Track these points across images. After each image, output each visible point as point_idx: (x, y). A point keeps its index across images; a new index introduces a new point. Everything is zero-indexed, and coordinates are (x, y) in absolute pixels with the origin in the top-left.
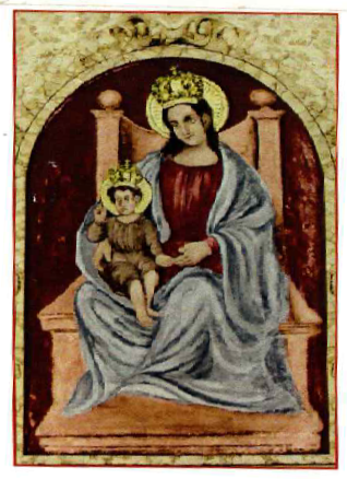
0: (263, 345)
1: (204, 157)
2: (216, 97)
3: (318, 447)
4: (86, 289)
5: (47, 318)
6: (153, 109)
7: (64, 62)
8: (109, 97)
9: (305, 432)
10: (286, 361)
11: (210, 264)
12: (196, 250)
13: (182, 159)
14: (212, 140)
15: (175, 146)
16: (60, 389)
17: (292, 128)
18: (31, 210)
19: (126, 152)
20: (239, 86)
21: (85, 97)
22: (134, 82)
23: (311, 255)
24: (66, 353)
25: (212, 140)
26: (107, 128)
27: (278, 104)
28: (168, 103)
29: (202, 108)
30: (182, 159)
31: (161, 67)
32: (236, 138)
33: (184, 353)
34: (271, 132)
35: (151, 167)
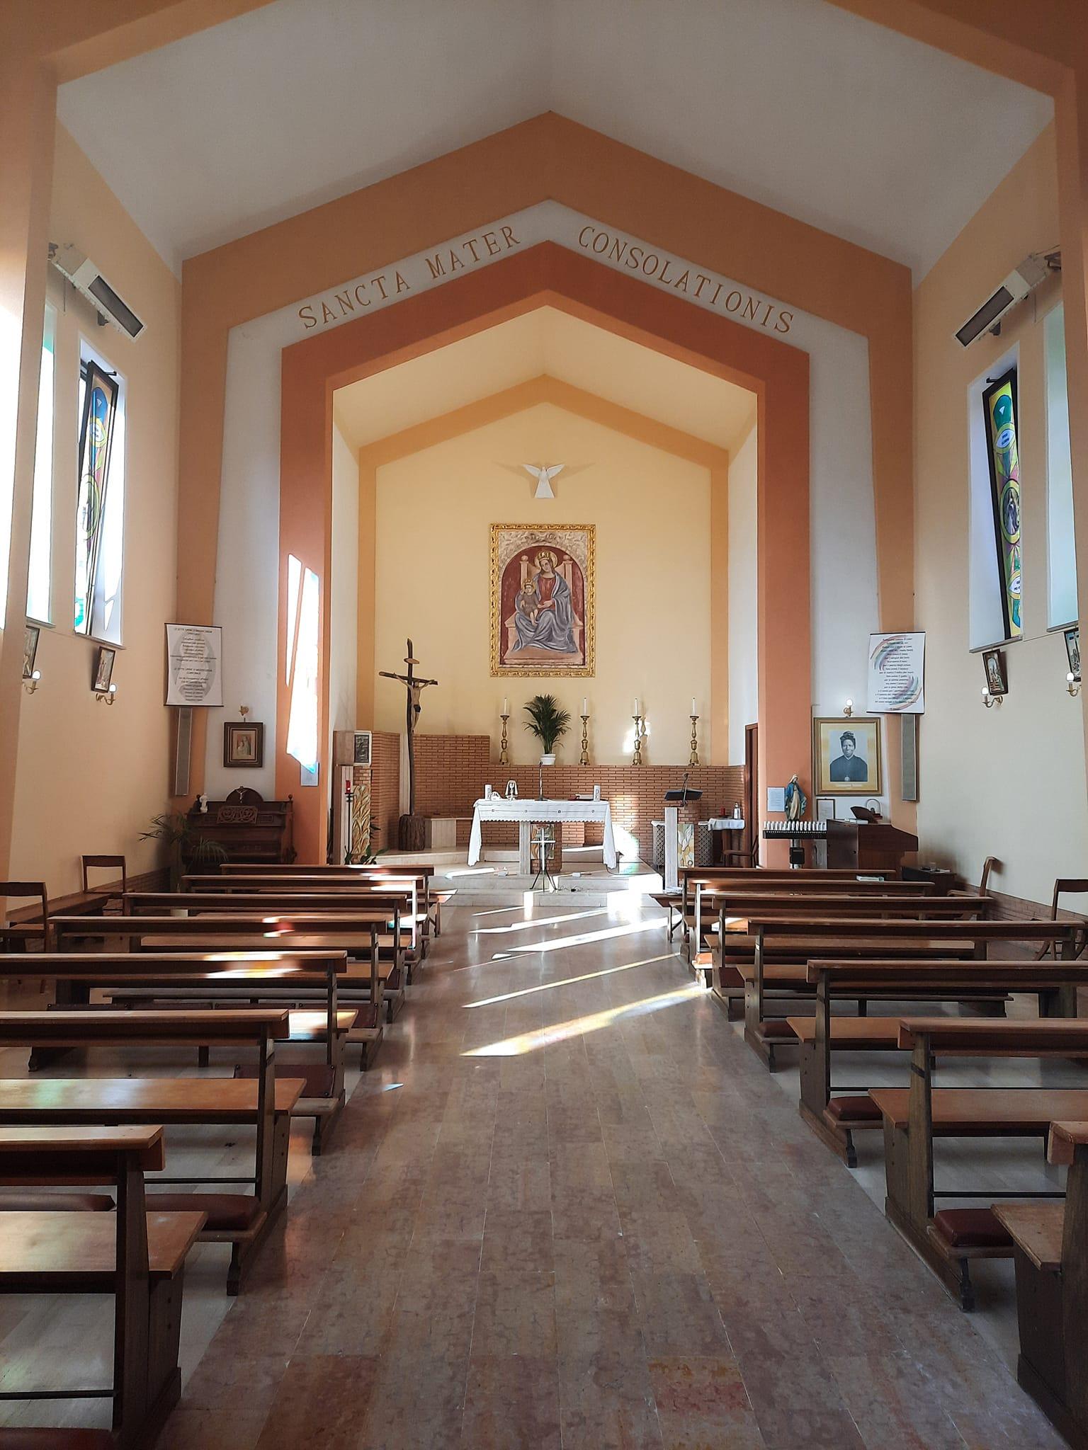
0: (567, 632)
1: (551, 576)
2: (554, 559)
3: (700, 477)
4: (517, 614)
5: (509, 623)
6: (537, 562)
7: (512, 547)
8: (525, 558)
9: (578, 659)
10: (929, 824)
11: (551, 608)
12: (548, 603)
13: (546, 576)
14: (554, 572)
15: (543, 572)
16: (511, 645)
17: (574, 564)
18: (223, 416)
19: (529, 573)
20: (560, 554)
21: (519, 557)
22: (532, 553)
23: (699, 1034)
24: (512, 635)
25: (554, 572)
26: (524, 567)
27: (571, 559)
28: (542, 560)
29: (550, 561)
30: (546, 576)
31: (540, 548)
32: (559, 569)
33: (545, 634)
34: (569, 568)
35: (536, 579)
